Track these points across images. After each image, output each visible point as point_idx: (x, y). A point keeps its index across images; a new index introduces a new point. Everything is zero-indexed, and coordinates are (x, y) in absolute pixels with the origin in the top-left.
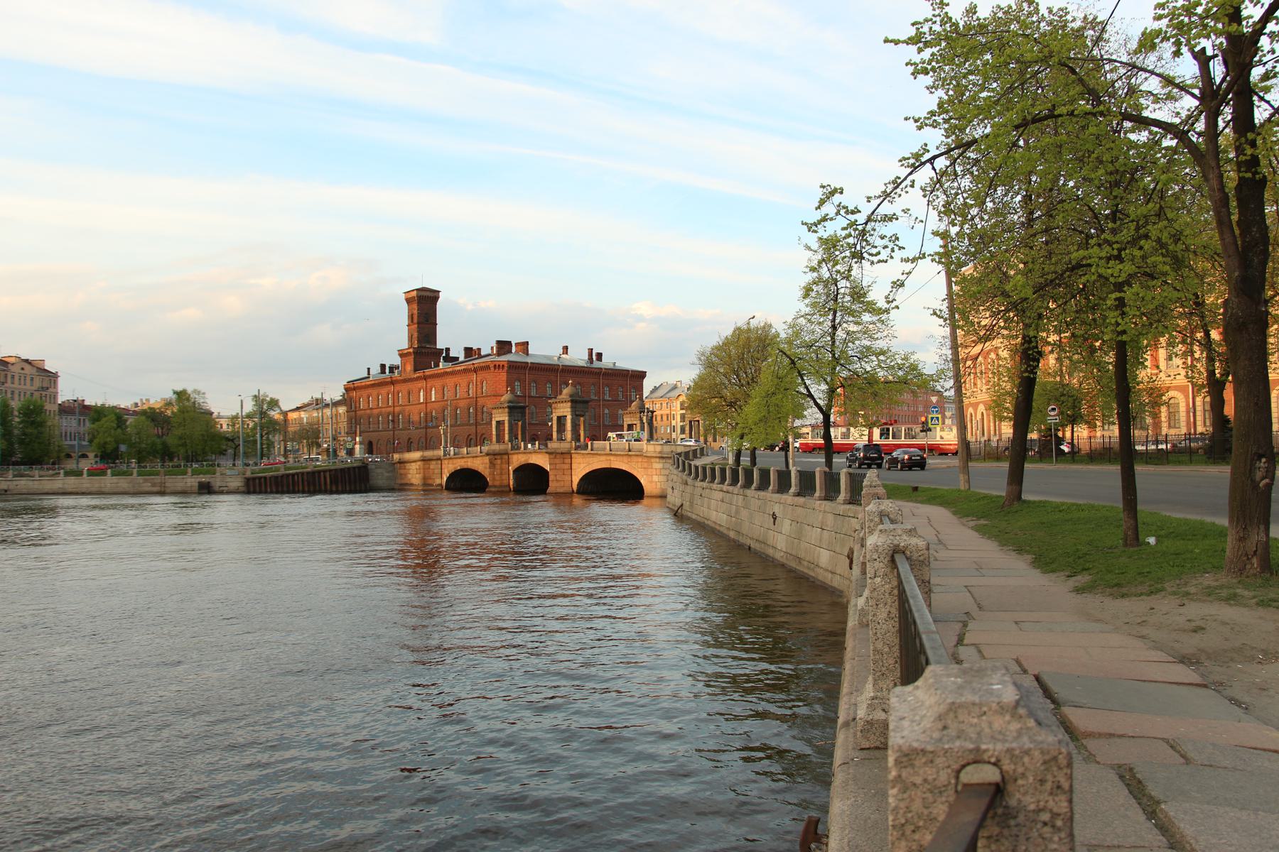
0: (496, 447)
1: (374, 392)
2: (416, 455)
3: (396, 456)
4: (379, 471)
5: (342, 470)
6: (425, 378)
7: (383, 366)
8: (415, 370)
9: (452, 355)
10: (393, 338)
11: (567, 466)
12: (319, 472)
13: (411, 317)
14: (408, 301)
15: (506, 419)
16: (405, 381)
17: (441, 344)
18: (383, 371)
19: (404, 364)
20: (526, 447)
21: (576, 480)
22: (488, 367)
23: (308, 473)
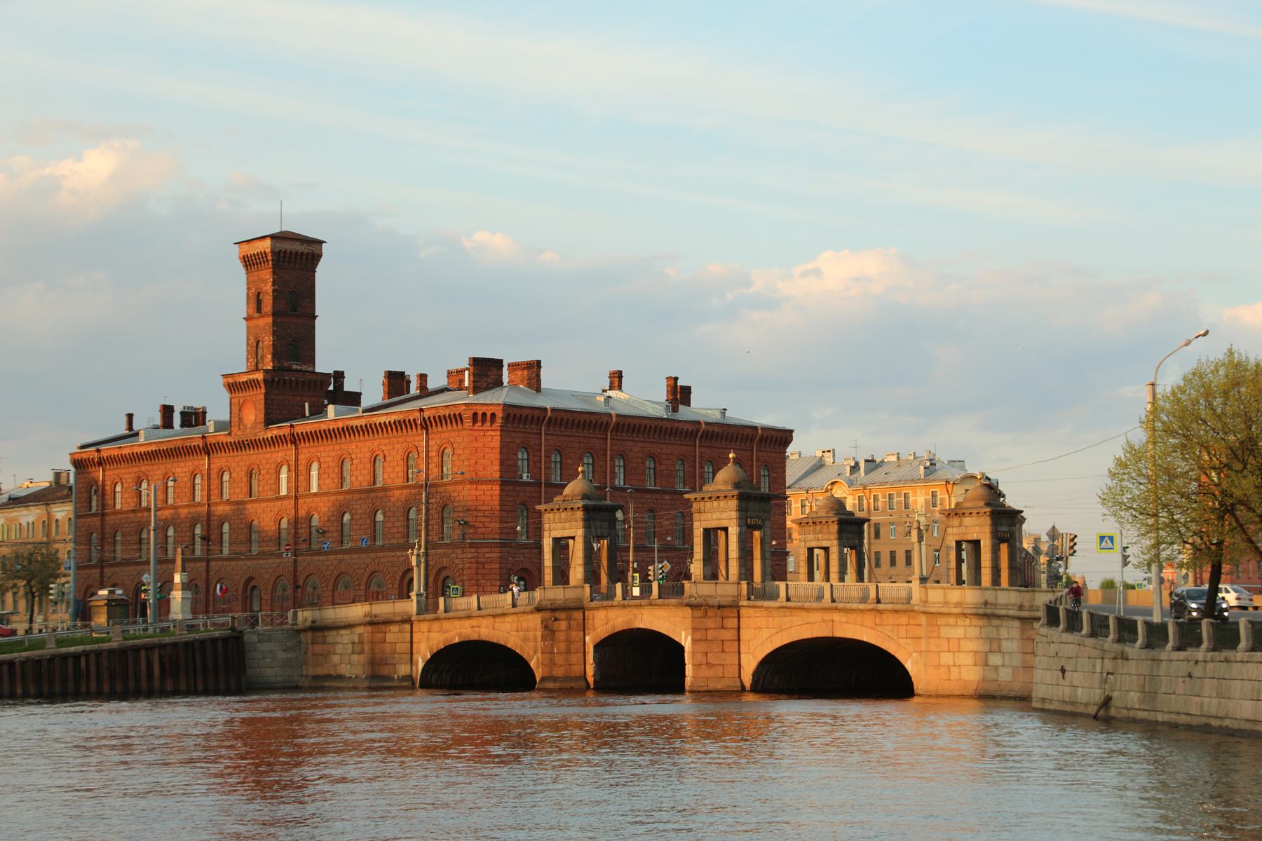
0: (557, 594)
1: (157, 469)
2: (357, 611)
3: (305, 616)
4: (266, 647)
5: (188, 645)
6: (295, 440)
7: (167, 411)
8: (269, 421)
9: (349, 386)
10: (207, 348)
11: (729, 635)
12: (136, 649)
13: (256, 301)
14: (249, 262)
15: (579, 533)
16: (240, 446)
17: (324, 364)
18: (167, 422)
19: (236, 410)
20: (626, 593)
21: (750, 665)
22: (458, 418)
23: (111, 652)
